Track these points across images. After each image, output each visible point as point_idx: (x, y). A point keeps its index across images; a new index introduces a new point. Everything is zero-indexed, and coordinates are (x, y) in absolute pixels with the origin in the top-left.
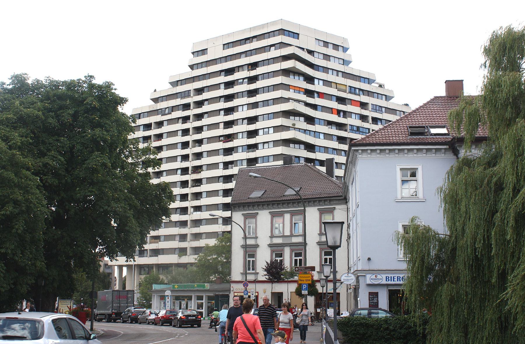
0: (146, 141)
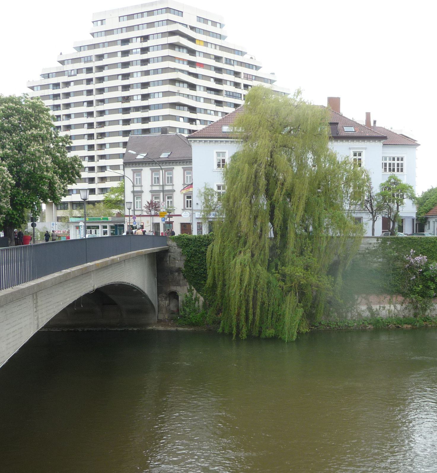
0: (56, 98)
